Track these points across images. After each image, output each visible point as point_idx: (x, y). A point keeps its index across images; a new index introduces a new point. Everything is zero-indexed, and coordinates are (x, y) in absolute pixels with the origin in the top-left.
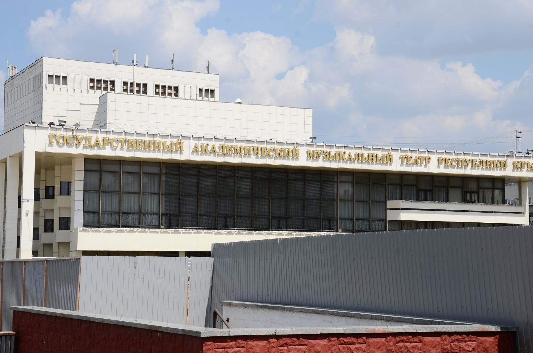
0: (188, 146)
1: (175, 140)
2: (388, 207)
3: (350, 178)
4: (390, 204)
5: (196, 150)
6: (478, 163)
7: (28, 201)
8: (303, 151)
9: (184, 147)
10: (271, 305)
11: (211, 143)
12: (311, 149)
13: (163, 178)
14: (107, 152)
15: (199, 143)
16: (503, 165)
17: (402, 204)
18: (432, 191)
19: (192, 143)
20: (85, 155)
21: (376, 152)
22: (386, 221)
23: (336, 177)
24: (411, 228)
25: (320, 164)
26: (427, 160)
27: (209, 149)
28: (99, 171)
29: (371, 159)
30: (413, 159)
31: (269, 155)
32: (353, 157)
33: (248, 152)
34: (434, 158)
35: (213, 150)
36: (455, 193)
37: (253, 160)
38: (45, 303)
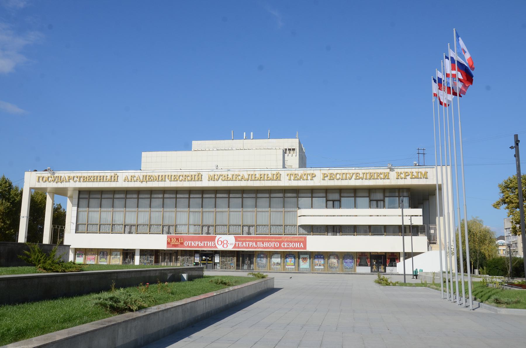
4: (301, 212)
7: (23, 217)
21: (266, 173)
26: (313, 176)
28: (297, 197)
33: (163, 180)
37: (168, 184)
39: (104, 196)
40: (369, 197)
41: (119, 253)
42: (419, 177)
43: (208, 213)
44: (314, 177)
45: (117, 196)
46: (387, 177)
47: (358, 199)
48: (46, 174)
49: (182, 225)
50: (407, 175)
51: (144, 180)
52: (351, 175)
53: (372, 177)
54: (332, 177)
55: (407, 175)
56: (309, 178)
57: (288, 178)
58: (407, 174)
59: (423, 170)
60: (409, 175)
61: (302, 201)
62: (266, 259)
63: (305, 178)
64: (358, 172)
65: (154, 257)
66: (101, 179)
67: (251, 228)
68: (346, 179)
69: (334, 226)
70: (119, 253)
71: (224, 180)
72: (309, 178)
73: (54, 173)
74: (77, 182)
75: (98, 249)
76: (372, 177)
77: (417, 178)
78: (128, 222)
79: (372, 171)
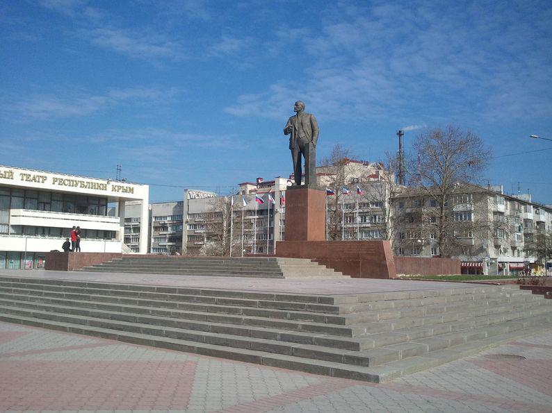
4: (13, 212)
6: (85, 184)
18: (50, 203)
26: (45, 179)
34: (50, 176)
40: (37, 199)
46: (105, 188)
53: (94, 186)
54: (62, 182)
56: (41, 180)
57: (21, 178)
59: (131, 186)
61: (14, 200)
63: (37, 179)
66: (75, 184)
69: (44, 228)
72: (41, 180)
76: (94, 186)
79: (94, 181)
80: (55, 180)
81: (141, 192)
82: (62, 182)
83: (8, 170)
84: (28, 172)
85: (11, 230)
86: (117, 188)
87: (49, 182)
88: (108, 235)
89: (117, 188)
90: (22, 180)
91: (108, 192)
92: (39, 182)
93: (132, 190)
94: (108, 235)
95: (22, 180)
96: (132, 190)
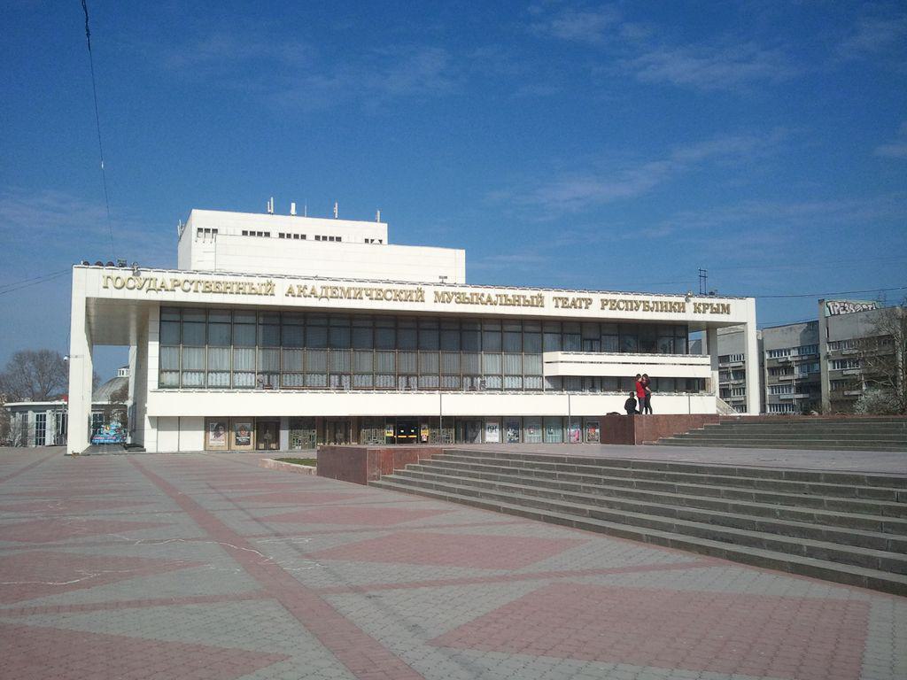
0: (281, 287)
1: (264, 280)
2: (545, 360)
3: (251, 319)
4: (547, 356)
5: (290, 292)
6: (651, 305)
7: (76, 357)
8: (429, 293)
9: (276, 290)
10: (703, 498)
11: (310, 284)
12: (440, 290)
13: (261, 328)
14: (179, 296)
15: (295, 283)
16: (682, 309)
17: (559, 355)
18: (599, 340)
19: (287, 283)
20: (161, 302)
22: (542, 377)
23: (479, 326)
24: (657, 387)
25: (453, 308)
26: (589, 302)
27: (485, 299)
29: (302, 292)
30: (570, 302)
31: (618, 307)
32: (494, 298)
33: (358, 297)
34: (597, 298)
35: (313, 292)
36: (219, 331)
37: (365, 304)
38: (836, 502)
39: (211, 318)
41: (249, 425)
42: (475, 301)
43: (196, 353)
44: (590, 304)
45: (239, 319)
47: (508, 336)
48: (125, 274)
49: (492, 375)
50: (706, 306)
51: (152, 287)
52: (143, 281)
53: (664, 307)
55: (176, 284)
58: (176, 283)
59: (725, 301)
60: (606, 305)
62: (202, 433)
64: (110, 275)
65: (316, 431)
67: (344, 378)
68: (632, 310)
70: (249, 425)
71: (459, 303)
72: (584, 305)
73: (137, 274)
74: (192, 291)
75: (582, 417)
76: (515, 302)
77: (718, 312)
78: (404, 370)
79: (664, 299)
80: (604, 303)
81: (743, 311)
82: (615, 305)
83: (535, 293)
84: (564, 294)
85: (547, 385)
86: (701, 308)
87: (596, 307)
88: (693, 385)
89: (701, 308)
90: (557, 307)
91: (689, 315)
92: (581, 308)
93: (726, 309)
94: (693, 385)
95: (557, 307)
96: (726, 309)
